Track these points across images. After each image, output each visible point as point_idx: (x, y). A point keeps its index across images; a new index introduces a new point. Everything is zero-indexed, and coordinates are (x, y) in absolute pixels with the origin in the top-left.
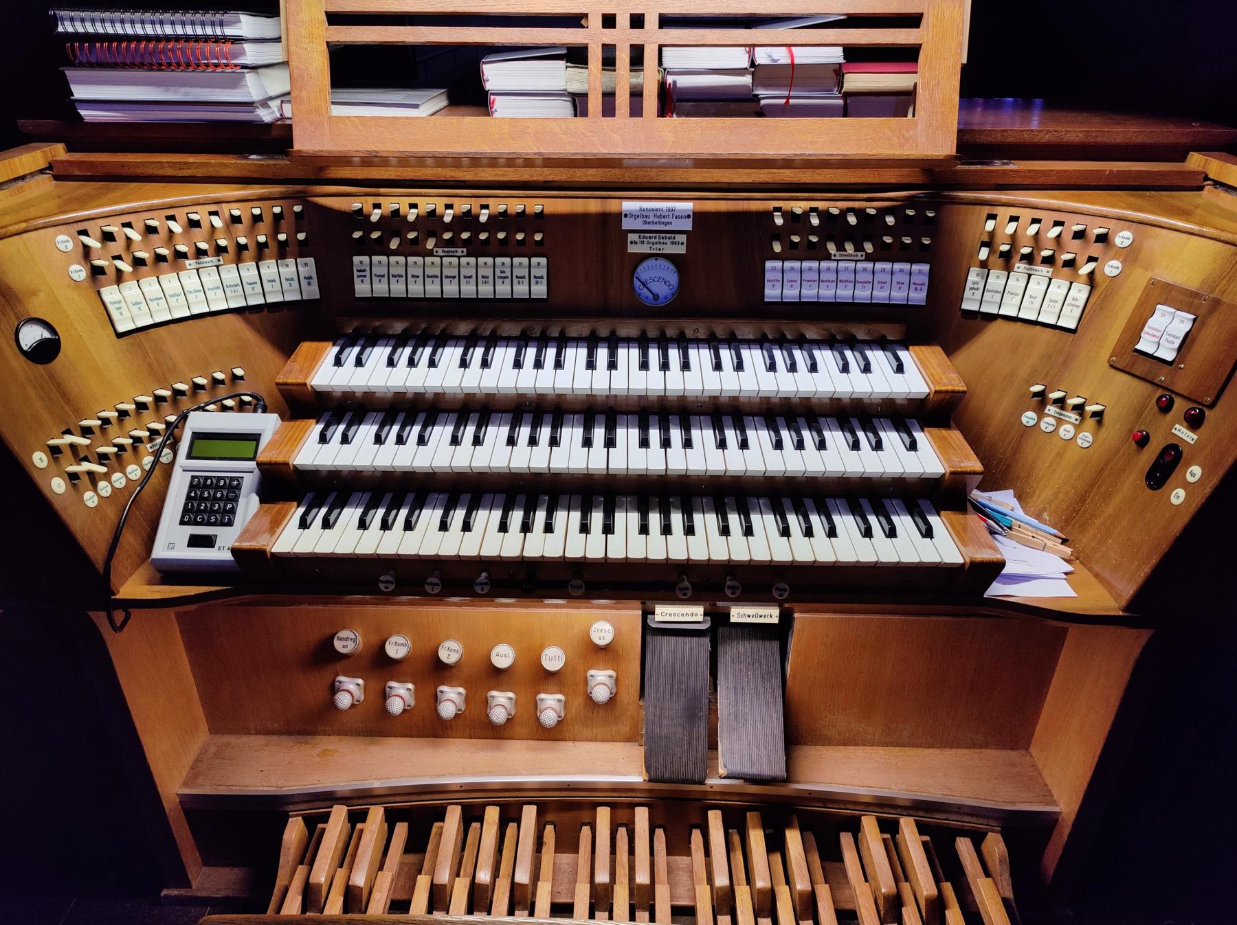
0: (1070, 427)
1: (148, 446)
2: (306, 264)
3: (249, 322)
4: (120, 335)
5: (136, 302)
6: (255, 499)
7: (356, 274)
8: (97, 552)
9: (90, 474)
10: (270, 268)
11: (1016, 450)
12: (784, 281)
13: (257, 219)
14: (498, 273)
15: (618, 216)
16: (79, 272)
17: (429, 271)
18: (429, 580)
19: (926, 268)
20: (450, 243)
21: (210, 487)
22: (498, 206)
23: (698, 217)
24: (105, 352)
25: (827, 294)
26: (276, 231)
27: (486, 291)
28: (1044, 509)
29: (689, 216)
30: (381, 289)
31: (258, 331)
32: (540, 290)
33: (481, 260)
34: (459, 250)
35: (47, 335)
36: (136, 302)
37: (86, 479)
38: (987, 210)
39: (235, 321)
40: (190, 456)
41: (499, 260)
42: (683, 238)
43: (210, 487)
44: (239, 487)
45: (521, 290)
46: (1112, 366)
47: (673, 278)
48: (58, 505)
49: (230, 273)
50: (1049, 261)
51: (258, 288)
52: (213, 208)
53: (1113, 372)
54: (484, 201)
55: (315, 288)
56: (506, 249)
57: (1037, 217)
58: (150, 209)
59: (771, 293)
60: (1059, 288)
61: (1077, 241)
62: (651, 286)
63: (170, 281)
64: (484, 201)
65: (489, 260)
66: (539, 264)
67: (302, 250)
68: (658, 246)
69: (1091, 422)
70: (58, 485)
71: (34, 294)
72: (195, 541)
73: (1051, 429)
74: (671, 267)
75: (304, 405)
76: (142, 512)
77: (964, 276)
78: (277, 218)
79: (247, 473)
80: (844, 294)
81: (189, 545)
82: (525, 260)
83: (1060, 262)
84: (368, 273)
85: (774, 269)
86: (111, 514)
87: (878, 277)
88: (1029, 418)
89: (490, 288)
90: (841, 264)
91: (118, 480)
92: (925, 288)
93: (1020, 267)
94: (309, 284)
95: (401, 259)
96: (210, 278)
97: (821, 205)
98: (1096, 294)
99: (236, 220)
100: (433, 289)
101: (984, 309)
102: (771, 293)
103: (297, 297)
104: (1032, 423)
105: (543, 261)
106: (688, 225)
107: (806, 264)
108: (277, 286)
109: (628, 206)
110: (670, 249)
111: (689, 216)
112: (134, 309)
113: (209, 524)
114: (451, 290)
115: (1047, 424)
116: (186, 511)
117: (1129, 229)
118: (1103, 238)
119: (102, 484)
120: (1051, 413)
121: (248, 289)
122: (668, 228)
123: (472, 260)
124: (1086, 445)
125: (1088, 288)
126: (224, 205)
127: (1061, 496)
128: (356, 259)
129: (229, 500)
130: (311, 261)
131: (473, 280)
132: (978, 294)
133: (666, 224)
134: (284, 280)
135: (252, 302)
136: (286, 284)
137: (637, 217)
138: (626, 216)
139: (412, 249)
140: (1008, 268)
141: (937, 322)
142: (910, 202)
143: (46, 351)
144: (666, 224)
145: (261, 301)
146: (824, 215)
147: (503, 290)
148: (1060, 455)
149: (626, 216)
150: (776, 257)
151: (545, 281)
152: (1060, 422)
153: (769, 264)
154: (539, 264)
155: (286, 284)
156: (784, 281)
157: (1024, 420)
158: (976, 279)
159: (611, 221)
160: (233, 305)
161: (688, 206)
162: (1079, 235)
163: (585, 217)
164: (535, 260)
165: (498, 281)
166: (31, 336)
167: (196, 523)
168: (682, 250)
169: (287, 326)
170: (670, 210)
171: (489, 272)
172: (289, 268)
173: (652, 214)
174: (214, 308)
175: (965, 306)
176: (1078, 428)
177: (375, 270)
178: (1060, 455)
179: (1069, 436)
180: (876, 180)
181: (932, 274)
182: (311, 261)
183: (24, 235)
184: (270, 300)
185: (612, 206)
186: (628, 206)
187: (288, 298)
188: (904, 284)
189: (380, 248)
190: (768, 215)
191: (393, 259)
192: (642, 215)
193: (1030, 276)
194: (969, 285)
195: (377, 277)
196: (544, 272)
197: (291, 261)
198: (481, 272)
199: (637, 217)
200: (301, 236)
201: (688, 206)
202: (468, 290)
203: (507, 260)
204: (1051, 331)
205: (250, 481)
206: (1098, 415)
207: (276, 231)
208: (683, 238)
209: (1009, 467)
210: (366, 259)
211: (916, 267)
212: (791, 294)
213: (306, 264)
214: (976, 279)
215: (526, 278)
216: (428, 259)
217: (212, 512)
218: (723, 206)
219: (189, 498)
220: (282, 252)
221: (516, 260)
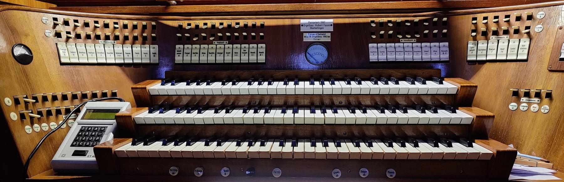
0: (536, 105)
1: (64, 116)
2: (154, 48)
3: (124, 70)
4: (62, 64)
5: (71, 52)
6: (112, 135)
7: (176, 52)
8: (25, 156)
9: (32, 118)
10: (137, 48)
11: (510, 123)
12: (378, 52)
13: (135, 27)
14: (242, 51)
15: (299, 26)
16: (50, 33)
17: (210, 51)
18: (196, 169)
19: (447, 44)
20: (221, 38)
21: (89, 131)
22: (242, 23)
23: (336, 25)
24: (53, 67)
25: (400, 57)
26: (143, 31)
27: (236, 59)
28: (532, 150)
29: (331, 25)
30: (187, 59)
31: (128, 76)
32: (262, 58)
33: (235, 46)
34: (225, 42)
35: (27, 53)
36: (71, 52)
37: (28, 120)
38: (472, 16)
39: (117, 69)
40: (82, 118)
41: (243, 46)
42: (330, 34)
43: (89, 131)
44: (104, 131)
45: (253, 59)
46: (550, 71)
47: (325, 53)
48: (11, 125)
49: (119, 48)
50: (506, 32)
51: (131, 56)
52: (116, 21)
53: (551, 73)
54: (238, 21)
55: (157, 58)
56: (246, 40)
57: (496, 15)
58: (87, 16)
59: (373, 57)
60: (514, 43)
61: (518, 22)
62: (314, 57)
63: (90, 46)
64: (238, 21)
65: (239, 46)
66: (262, 47)
67: (154, 41)
68: (318, 38)
69: (546, 100)
70: (14, 116)
71: (27, 35)
72: (76, 153)
73: (526, 109)
74: (322, 47)
75: (144, 101)
76: (51, 141)
77: (466, 47)
78: (144, 27)
79: (110, 124)
80: (408, 57)
81: (73, 155)
82: (255, 45)
83: (512, 31)
84: (182, 52)
85: (373, 47)
86: (37, 141)
87: (424, 49)
88: (513, 106)
89: (238, 58)
90: (405, 44)
91: (45, 126)
92: (448, 52)
93: (493, 38)
94: (154, 56)
95: (198, 46)
96: (109, 49)
97: (393, 19)
98: (533, 41)
99: (125, 26)
100: (211, 59)
101: (479, 58)
102: (373, 57)
103: (148, 61)
104: (515, 108)
105: (264, 45)
106: (331, 29)
107: (388, 45)
108: (139, 56)
109: (303, 21)
110: (323, 39)
111: (331, 25)
112: (71, 55)
113: (86, 146)
114: (220, 59)
115: (523, 107)
116: (75, 140)
117: (542, 11)
118: (530, 17)
119: (36, 125)
120: (524, 101)
121: (126, 56)
122: (322, 30)
123: (231, 46)
124: (546, 111)
125: (529, 39)
126: (121, 21)
127: (540, 141)
128: (177, 46)
129: (98, 136)
130: (156, 46)
131: (231, 54)
132: (475, 53)
133: (321, 28)
134: (142, 53)
135: (126, 61)
136: (143, 56)
137: (307, 26)
138: (302, 25)
139: (204, 41)
140: (487, 39)
141: (457, 66)
142: (435, 16)
143: (25, 60)
144: (321, 28)
145: (131, 61)
146: (395, 23)
147: (245, 59)
148: (534, 120)
149: (302, 25)
150: (374, 41)
151: (264, 54)
152: (529, 104)
153: (370, 45)
154: (262, 47)
155: (143, 56)
156: (378, 52)
157: (510, 107)
158: (472, 46)
159: (295, 30)
160: (118, 61)
161: (331, 21)
162: (518, 19)
163: (284, 27)
164: (260, 45)
165: (242, 55)
166: (19, 51)
167: (79, 146)
168: (329, 40)
169: (142, 72)
170: (322, 23)
171: (238, 51)
172: (146, 49)
173: (314, 25)
174: (109, 61)
175: (469, 59)
176: (540, 104)
177: (185, 51)
178: (534, 120)
179: (536, 110)
180: (417, 7)
181: (450, 46)
182: (156, 46)
183: (29, 12)
184: (135, 61)
185: (296, 22)
186: (303, 21)
187: (144, 61)
188: (437, 52)
189: (189, 41)
190: (368, 24)
191: (194, 46)
192: (309, 25)
193: (498, 41)
194: (469, 49)
195: (186, 54)
196: (264, 50)
197: (147, 46)
198: (234, 51)
199: (307, 26)
200: (153, 35)
201: (331, 21)
202: (228, 59)
203: (247, 46)
204: (515, 63)
205: (110, 128)
206: (549, 95)
207: (143, 31)
208: (329, 34)
209: (508, 133)
210: (182, 46)
211: (441, 44)
212: (382, 58)
213: (154, 48)
214: (472, 46)
215: (256, 54)
216: (210, 46)
217: (89, 141)
218: (347, 21)
219: (78, 135)
220: (145, 41)
221: (251, 45)
